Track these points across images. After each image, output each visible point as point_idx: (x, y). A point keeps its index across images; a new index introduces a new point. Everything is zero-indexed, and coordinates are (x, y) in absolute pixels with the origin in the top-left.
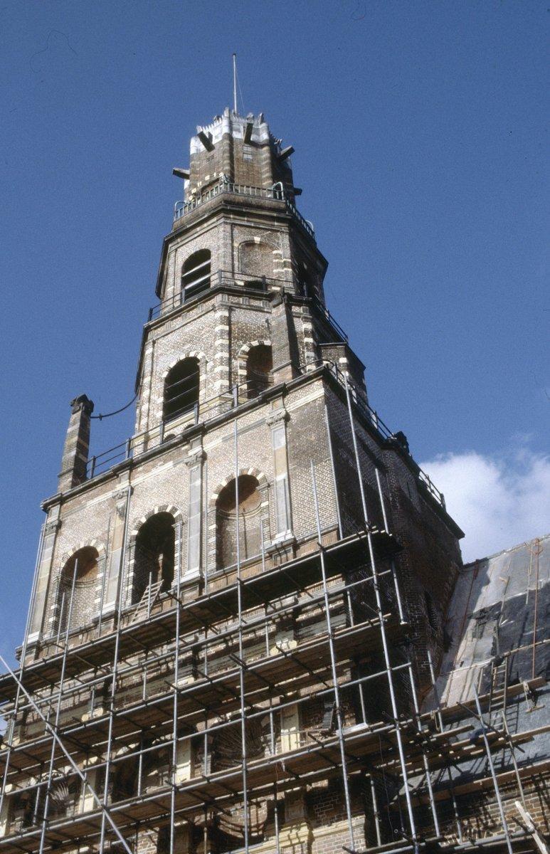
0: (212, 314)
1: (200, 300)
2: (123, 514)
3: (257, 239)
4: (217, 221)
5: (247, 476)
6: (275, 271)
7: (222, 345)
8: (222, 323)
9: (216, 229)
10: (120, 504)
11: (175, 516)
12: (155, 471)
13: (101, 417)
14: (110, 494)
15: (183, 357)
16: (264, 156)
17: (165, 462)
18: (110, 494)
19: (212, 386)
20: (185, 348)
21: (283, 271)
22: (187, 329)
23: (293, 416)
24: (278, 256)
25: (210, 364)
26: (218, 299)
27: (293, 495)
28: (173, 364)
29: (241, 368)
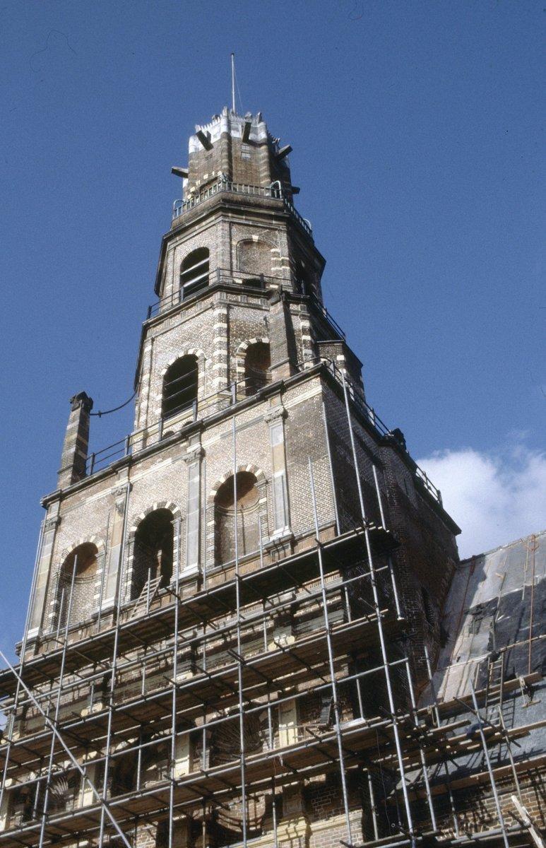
0: (210, 311)
1: (198, 298)
2: (122, 510)
3: (255, 238)
4: (216, 219)
5: (245, 472)
6: (273, 269)
7: (220, 342)
8: (220, 321)
9: (215, 227)
10: (120, 500)
11: (173, 512)
12: (154, 468)
13: (100, 414)
14: (109, 491)
15: (181, 354)
16: (262, 155)
17: (164, 458)
18: (109, 491)
19: (210, 383)
20: (184, 345)
21: (281, 269)
22: (185, 327)
23: (291, 413)
24: (276, 254)
25: (209, 361)
26: (216, 297)
27: (291, 491)
28: (171, 362)
29: (239, 365)
